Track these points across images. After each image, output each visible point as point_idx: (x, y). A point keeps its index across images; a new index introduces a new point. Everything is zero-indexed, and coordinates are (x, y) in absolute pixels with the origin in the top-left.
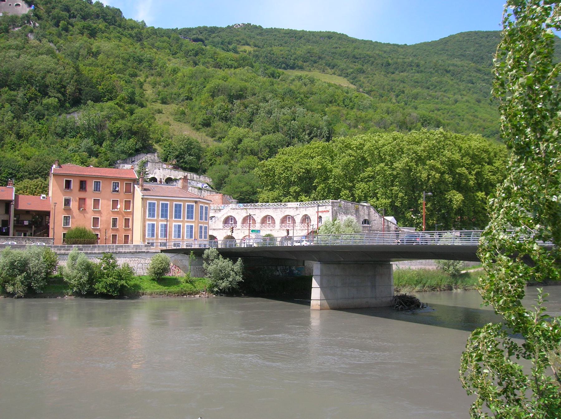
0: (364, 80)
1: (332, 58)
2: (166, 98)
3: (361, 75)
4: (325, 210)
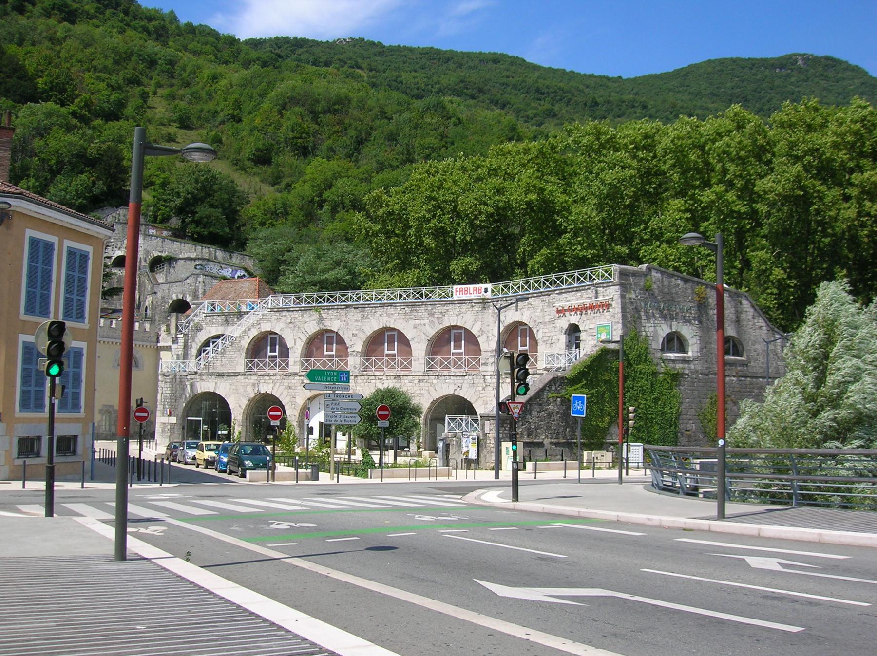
1: (501, 91)
2: (189, 118)
3: (550, 120)
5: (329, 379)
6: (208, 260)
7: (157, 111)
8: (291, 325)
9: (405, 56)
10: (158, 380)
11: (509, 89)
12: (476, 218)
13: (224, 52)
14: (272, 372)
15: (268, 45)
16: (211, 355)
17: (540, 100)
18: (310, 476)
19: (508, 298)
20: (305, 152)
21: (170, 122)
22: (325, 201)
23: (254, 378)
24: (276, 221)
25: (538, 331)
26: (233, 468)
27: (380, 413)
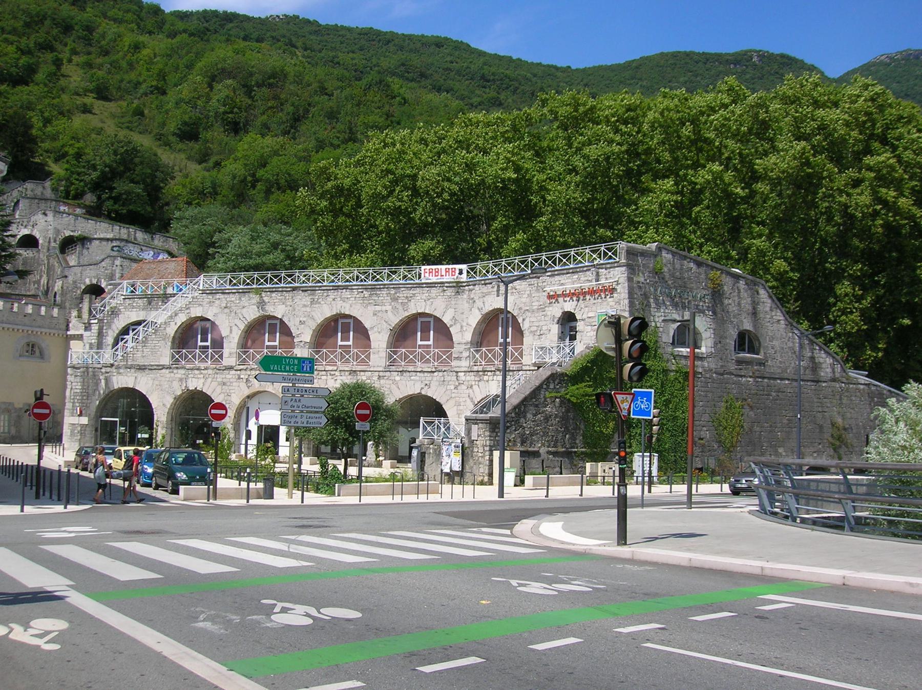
2: (107, 88)
5: (287, 368)
6: (127, 241)
7: (72, 80)
8: (226, 310)
9: (343, 36)
10: (66, 374)
11: (452, 74)
13: (148, 21)
14: (202, 366)
15: (195, 18)
16: (130, 344)
17: (485, 87)
18: (262, 493)
19: (487, 281)
20: (236, 128)
21: (87, 91)
22: (258, 181)
23: (182, 371)
24: (203, 201)
25: (524, 320)
26: (161, 481)
27: (359, 412)
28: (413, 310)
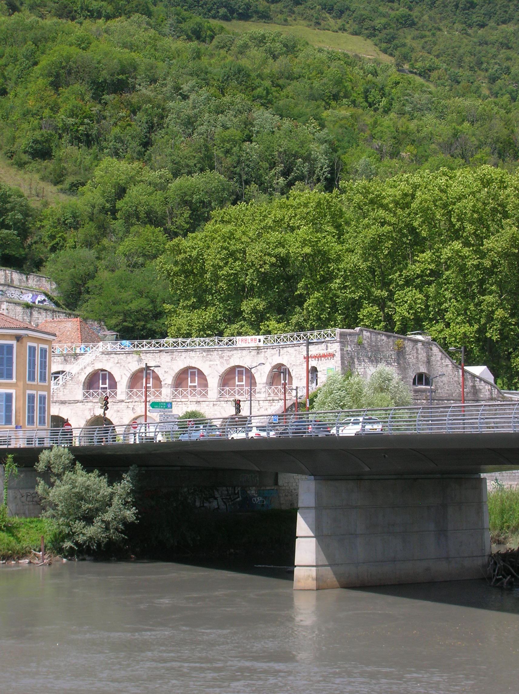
0: (414, 44)
4: (325, 352)
8: (118, 365)
12: (261, 267)
23: (90, 404)
28: (232, 364)
